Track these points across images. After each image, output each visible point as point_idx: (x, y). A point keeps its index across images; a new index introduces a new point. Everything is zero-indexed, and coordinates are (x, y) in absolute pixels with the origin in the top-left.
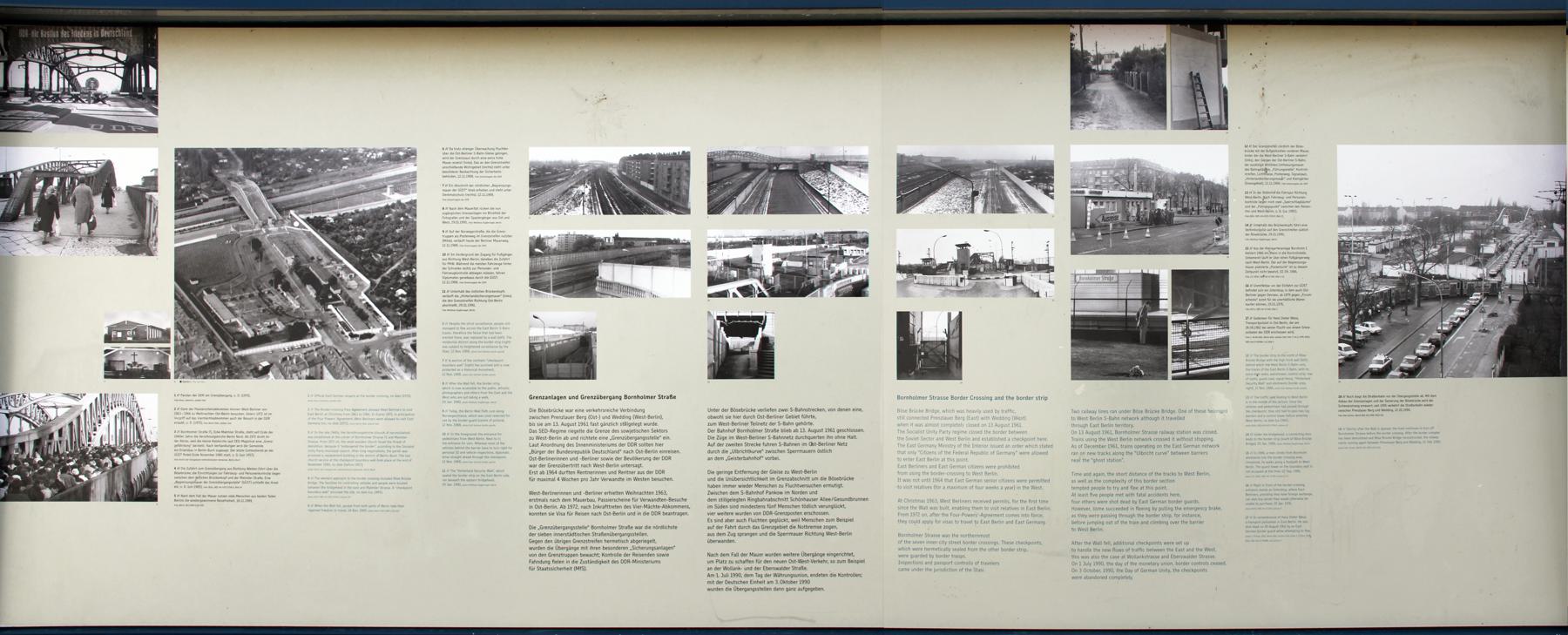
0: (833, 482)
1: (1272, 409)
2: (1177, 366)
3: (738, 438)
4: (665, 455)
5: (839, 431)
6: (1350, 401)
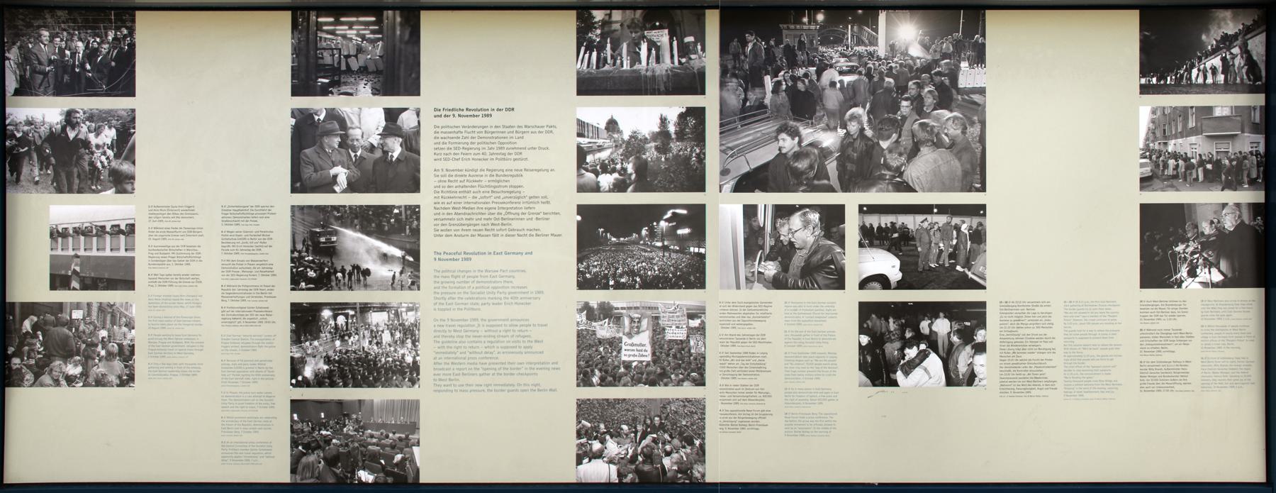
0: (471, 113)
1: (231, 398)
2: (1181, 353)
3: (502, 224)
4: (517, 151)
5: (1102, 356)
6: (1029, 385)
